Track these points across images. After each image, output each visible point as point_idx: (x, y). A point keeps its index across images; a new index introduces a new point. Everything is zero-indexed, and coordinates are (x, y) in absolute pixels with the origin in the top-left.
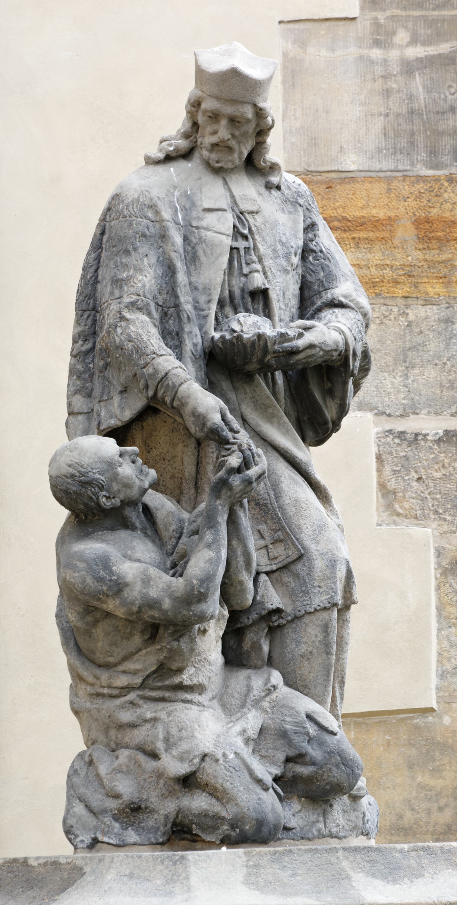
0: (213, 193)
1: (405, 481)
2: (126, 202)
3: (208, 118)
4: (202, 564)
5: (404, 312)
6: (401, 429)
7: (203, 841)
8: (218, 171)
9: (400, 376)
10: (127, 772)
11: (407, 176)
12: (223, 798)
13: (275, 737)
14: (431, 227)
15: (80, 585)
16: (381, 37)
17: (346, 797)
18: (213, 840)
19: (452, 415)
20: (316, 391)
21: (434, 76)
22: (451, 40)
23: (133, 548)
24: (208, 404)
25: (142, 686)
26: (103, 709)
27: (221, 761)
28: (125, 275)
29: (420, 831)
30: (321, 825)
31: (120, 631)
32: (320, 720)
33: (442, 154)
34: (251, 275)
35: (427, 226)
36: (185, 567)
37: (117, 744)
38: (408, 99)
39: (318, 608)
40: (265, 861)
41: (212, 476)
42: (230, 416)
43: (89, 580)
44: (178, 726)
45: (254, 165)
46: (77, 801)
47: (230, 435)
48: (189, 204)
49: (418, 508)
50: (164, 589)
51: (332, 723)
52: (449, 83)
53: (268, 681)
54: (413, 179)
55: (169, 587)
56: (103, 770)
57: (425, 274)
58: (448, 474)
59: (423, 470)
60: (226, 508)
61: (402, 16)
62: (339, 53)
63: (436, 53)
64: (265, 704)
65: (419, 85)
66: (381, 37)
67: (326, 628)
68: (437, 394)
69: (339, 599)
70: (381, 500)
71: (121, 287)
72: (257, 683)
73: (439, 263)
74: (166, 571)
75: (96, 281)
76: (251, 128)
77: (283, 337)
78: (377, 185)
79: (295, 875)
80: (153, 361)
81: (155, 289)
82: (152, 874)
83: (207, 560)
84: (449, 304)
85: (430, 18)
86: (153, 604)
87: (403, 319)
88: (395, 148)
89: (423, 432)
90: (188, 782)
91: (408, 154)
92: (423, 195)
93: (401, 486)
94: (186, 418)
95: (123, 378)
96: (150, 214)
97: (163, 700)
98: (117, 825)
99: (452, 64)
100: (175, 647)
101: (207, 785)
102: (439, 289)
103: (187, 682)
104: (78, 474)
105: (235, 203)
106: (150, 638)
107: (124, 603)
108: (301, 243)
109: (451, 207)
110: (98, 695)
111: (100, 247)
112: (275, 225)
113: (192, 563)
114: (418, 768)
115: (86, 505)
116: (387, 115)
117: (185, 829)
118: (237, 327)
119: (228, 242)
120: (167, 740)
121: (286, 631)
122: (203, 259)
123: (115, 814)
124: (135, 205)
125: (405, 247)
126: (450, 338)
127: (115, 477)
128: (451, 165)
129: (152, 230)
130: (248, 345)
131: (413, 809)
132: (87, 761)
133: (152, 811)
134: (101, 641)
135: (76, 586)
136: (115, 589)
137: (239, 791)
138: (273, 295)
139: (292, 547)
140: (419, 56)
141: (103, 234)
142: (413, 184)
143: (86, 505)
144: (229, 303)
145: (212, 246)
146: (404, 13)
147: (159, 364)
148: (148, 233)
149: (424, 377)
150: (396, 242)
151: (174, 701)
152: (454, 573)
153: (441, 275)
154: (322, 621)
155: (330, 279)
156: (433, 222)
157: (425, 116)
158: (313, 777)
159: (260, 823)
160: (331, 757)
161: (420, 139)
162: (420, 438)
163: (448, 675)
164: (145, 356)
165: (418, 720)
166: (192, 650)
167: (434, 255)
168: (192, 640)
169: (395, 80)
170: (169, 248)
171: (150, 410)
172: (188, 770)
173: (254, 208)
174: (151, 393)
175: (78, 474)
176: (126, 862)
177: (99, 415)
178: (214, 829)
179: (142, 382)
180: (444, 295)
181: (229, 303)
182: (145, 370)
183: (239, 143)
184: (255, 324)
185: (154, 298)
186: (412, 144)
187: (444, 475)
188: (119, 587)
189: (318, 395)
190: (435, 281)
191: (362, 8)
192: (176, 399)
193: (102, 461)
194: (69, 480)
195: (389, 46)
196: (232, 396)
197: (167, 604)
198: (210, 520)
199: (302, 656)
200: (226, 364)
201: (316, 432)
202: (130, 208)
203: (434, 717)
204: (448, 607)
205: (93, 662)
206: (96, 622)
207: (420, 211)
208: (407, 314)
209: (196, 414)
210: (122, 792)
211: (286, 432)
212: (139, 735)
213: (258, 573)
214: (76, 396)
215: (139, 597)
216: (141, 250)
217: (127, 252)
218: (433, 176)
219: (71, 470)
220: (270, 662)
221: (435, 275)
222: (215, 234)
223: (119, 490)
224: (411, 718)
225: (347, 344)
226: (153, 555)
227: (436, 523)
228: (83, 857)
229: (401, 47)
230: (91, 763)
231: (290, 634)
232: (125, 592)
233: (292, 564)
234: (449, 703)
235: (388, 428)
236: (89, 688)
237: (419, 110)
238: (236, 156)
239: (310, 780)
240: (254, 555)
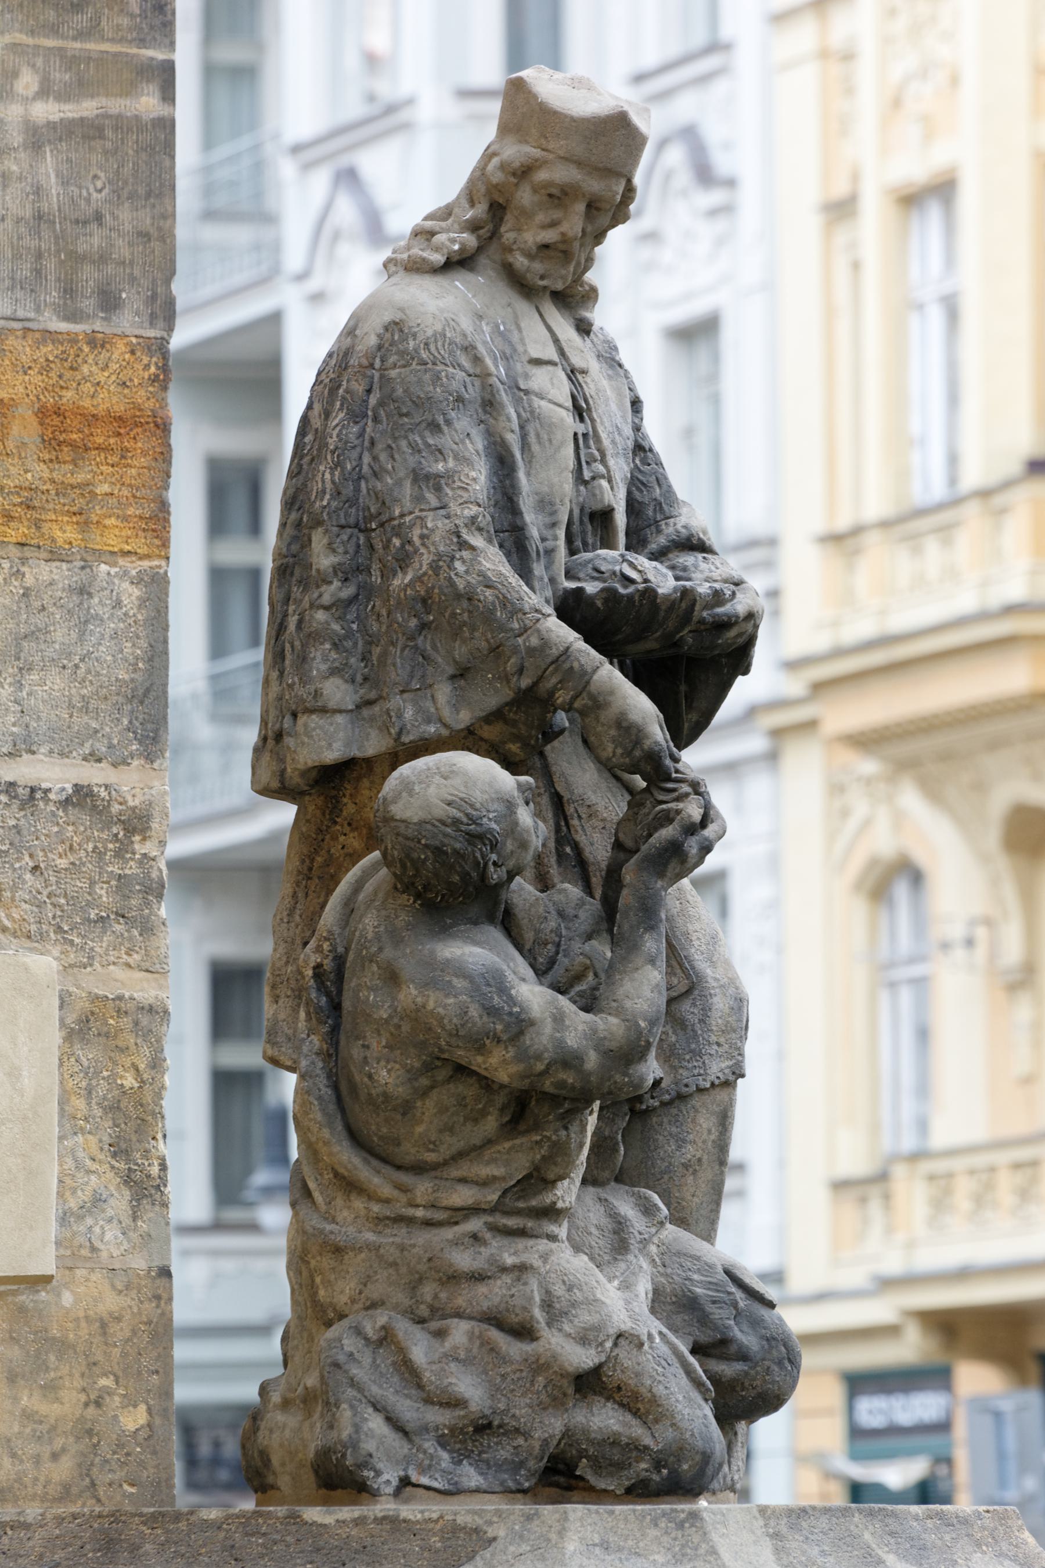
1: (15, 870)
2: (421, 337)
3: (545, 198)
5: (18, 571)
6: (9, 778)
7: (592, 1489)
9: (10, 684)
10: (466, 1362)
11: (29, 329)
12: (648, 1412)
13: (669, 1308)
14: (62, 423)
15: (455, 1020)
18: (612, 1488)
19: (85, 759)
22: (98, 95)
25: (495, 1208)
26: (414, 1246)
27: (646, 1347)
29: (23, 1493)
31: (465, 1106)
33: (82, 296)
34: (596, 482)
35: (56, 421)
38: (33, 194)
39: (717, 1082)
43: (474, 1011)
44: (564, 1282)
46: (370, 1410)
49: (32, 920)
50: (586, 1034)
54: (37, 335)
55: (595, 1031)
57: (51, 506)
58: (77, 863)
59: (41, 854)
61: (28, 46)
63: (75, 115)
65: (51, 171)
68: (65, 719)
73: (73, 487)
80: (538, 625)
82: (641, 1544)
84: (85, 561)
85: (69, 54)
87: (16, 583)
88: (13, 279)
89: (44, 785)
90: (590, 1384)
91: (32, 291)
92: (52, 365)
97: (522, 1233)
98: (445, 1455)
99: (100, 137)
100: (564, 1138)
101: (619, 1388)
104: (465, 820)
106: (510, 1122)
107: (523, 1056)
109: (92, 390)
110: (400, 1220)
114: (22, 1382)
117: (561, 1466)
120: (549, 1306)
121: (655, 1119)
123: (443, 1435)
124: (440, 344)
125: (23, 455)
126: (86, 622)
128: (95, 315)
130: (664, 607)
131: (14, 1455)
135: (446, 1021)
136: (514, 1029)
137: (677, 1401)
139: (679, 971)
140: (51, 118)
142: (38, 344)
145: (550, 426)
146: (30, 41)
147: (549, 630)
148: (467, 396)
149: (45, 688)
151: (537, 1237)
152: (83, 1039)
153: (75, 509)
154: (719, 1105)
156: (67, 414)
157: (58, 226)
158: (738, 1380)
160: (771, 1347)
161: (50, 265)
162: (39, 795)
163: (72, 1219)
164: (520, 615)
165: (24, 1297)
167: (63, 473)
169: (15, 158)
170: (502, 424)
172: (597, 1361)
175: (465, 820)
176: (589, 1521)
179: (513, 660)
180: (79, 546)
182: (520, 640)
186: (38, 272)
187: (72, 863)
190: (66, 519)
192: (584, 694)
194: (449, 830)
195: (7, 96)
197: (592, 1060)
199: (686, 1166)
202: (432, 348)
203: (48, 1293)
204: (73, 1098)
207: (46, 393)
208: (24, 575)
209: (624, 724)
210: (467, 1395)
214: (332, 680)
215: (550, 1046)
216: (458, 425)
217: (435, 427)
218: (68, 334)
219: (454, 812)
221: (66, 508)
222: (551, 406)
223: (512, 852)
224: (14, 1293)
227: (59, 948)
229: (26, 100)
232: (527, 1037)
234: (70, 1269)
237: (49, 214)
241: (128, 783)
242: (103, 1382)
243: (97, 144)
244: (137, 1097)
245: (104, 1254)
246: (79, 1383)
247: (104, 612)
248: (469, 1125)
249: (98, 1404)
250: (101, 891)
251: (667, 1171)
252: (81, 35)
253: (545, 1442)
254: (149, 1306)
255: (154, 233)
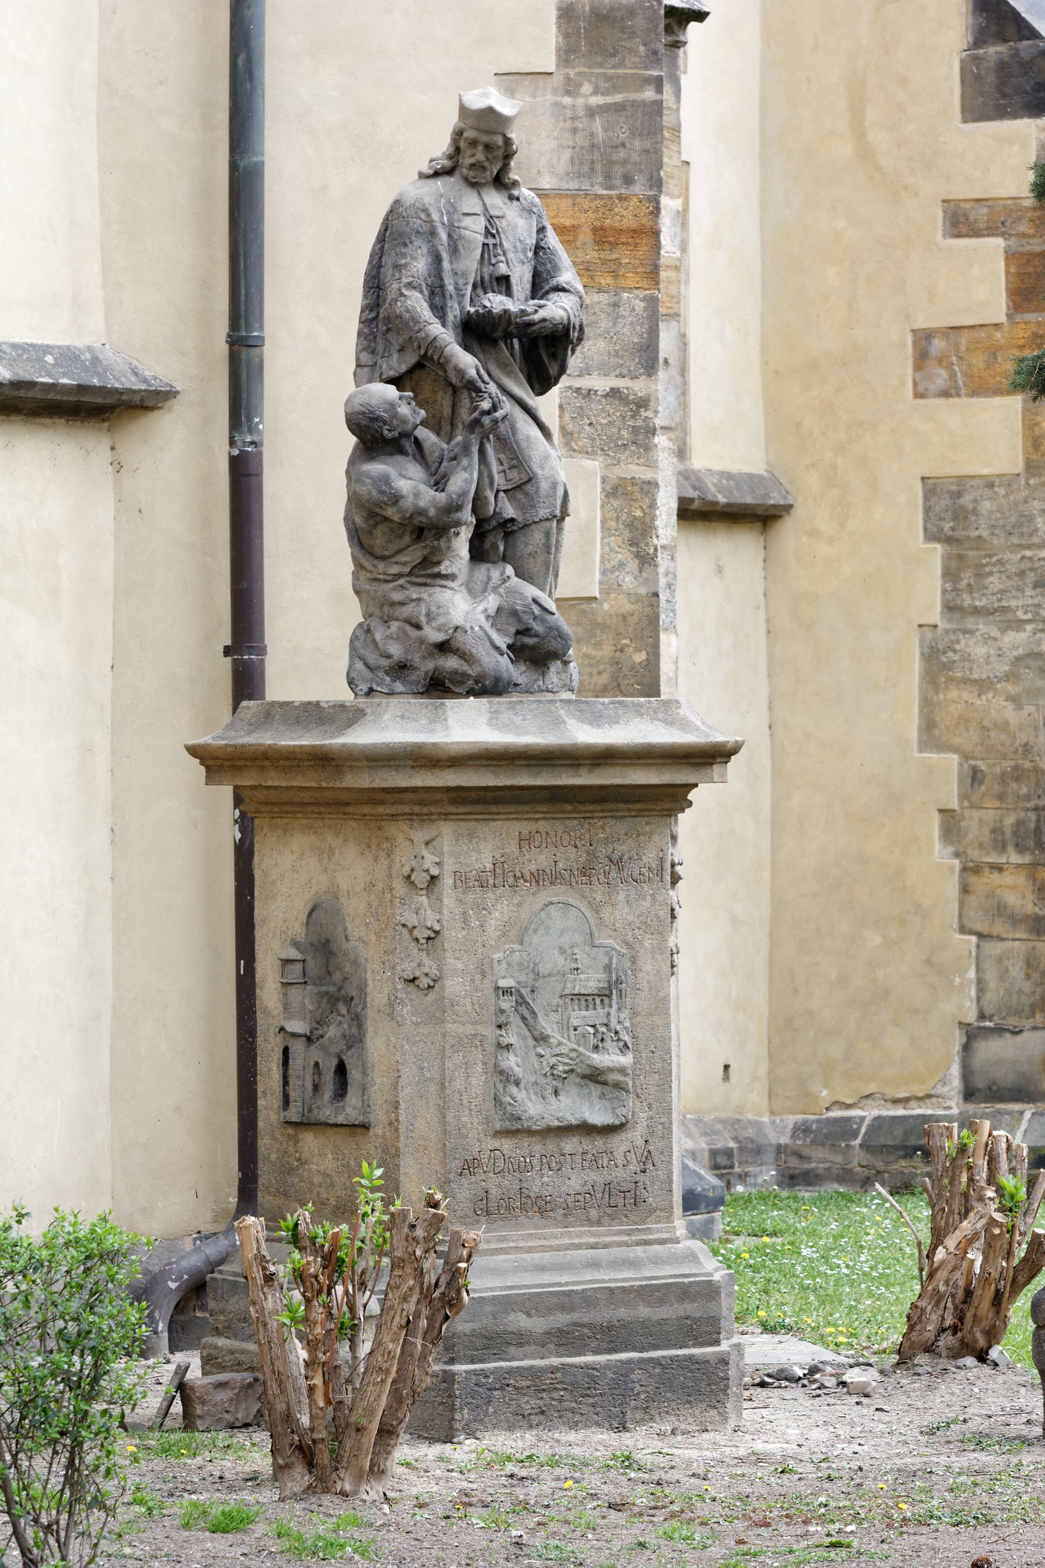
0: (470, 202)
4: (460, 483)
6: (578, 386)
8: (474, 185)
10: (397, 639)
16: (571, 88)
17: (559, 662)
20: (543, 353)
21: (610, 119)
23: (406, 469)
24: (467, 361)
25: (410, 574)
28: (403, 262)
30: (541, 683)
32: (543, 603)
35: (602, 232)
36: (446, 485)
37: (389, 617)
40: (503, 708)
41: (465, 415)
42: (482, 372)
43: (374, 493)
45: (500, 182)
47: (482, 385)
48: (452, 209)
51: (552, 606)
52: (621, 124)
53: (503, 572)
55: (434, 499)
56: (378, 636)
60: (478, 441)
62: (539, 99)
64: (501, 590)
66: (571, 88)
67: (548, 534)
69: (558, 513)
70: (562, 439)
71: (400, 271)
72: (495, 574)
74: (431, 487)
75: (380, 267)
76: (500, 153)
77: (523, 312)
78: (564, 201)
79: (525, 719)
81: (426, 273)
83: (463, 480)
86: (421, 512)
90: (444, 647)
93: (576, 429)
94: (449, 371)
95: (401, 340)
96: (423, 216)
97: (425, 585)
98: (388, 678)
102: (609, 280)
103: (444, 572)
105: (486, 209)
107: (400, 511)
108: (534, 242)
110: (375, 580)
111: (384, 240)
112: (515, 227)
113: (452, 481)
115: (373, 435)
116: (574, 148)
118: (488, 304)
119: (481, 239)
122: (462, 251)
127: (395, 415)
129: (424, 228)
132: (364, 631)
133: (416, 669)
134: (379, 539)
136: (394, 500)
138: (514, 280)
141: (386, 230)
142: (592, 200)
143: (373, 435)
144: (482, 285)
146: (588, 71)
150: (578, 244)
155: (556, 269)
159: (497, 680)
161: (598, 167)
166: (449, 548)
167: (606, 255)
168: (449, 540)
171: (419, 366)
173: (500, 214)
174: (422, 352)
177: (381, 368)
178: (462, 683)
181: (482, 285)
183: (491, 164)
184: (501, 302)
185: (425, 280)
186: (592, 170)
188: (396, 499)
189: (545, 358)
191: (557, 66)
193: (386, 402)
196: (481, 356)
197: (432, 512)
198: (466, 449)
199: (529, 555)
200: (478, 332)
201: (541, 385)
205: (372, 555)
206: (375, 526)
211: (520, 385)
212: (407, 611)
213: (498, 491)
216: (415, 243)
217: (405, 245)
219: (362, 409)
220: (505, 559)
224: (579, 604)
225: (569, 319)
226: (421, 475)
228: (361, 701)
229: (586, 96)
230: (368, 631)
231: (520, 538)
233: (523, 486)
235: (568, 385)
236: (368, 575)
238: (488, 174)
239: (534, 648)
240: (496, 477)
241: (639, 387)
242: (624, 641)
243: (623, 113)
244: (642, 520)
245: (625, 588)
246: (612, 642)
247: (626, 314)
248: (398, 540)
249: (621, 650)
250: (624, 433)
251: (522, 557)
252: (614, 67)
253: (426, 673)
254: (648, 610)
255: (652, 150)
